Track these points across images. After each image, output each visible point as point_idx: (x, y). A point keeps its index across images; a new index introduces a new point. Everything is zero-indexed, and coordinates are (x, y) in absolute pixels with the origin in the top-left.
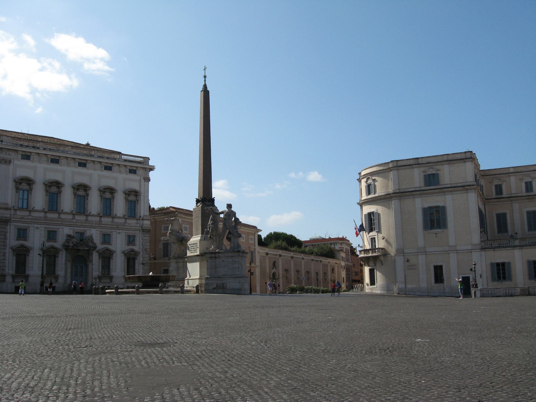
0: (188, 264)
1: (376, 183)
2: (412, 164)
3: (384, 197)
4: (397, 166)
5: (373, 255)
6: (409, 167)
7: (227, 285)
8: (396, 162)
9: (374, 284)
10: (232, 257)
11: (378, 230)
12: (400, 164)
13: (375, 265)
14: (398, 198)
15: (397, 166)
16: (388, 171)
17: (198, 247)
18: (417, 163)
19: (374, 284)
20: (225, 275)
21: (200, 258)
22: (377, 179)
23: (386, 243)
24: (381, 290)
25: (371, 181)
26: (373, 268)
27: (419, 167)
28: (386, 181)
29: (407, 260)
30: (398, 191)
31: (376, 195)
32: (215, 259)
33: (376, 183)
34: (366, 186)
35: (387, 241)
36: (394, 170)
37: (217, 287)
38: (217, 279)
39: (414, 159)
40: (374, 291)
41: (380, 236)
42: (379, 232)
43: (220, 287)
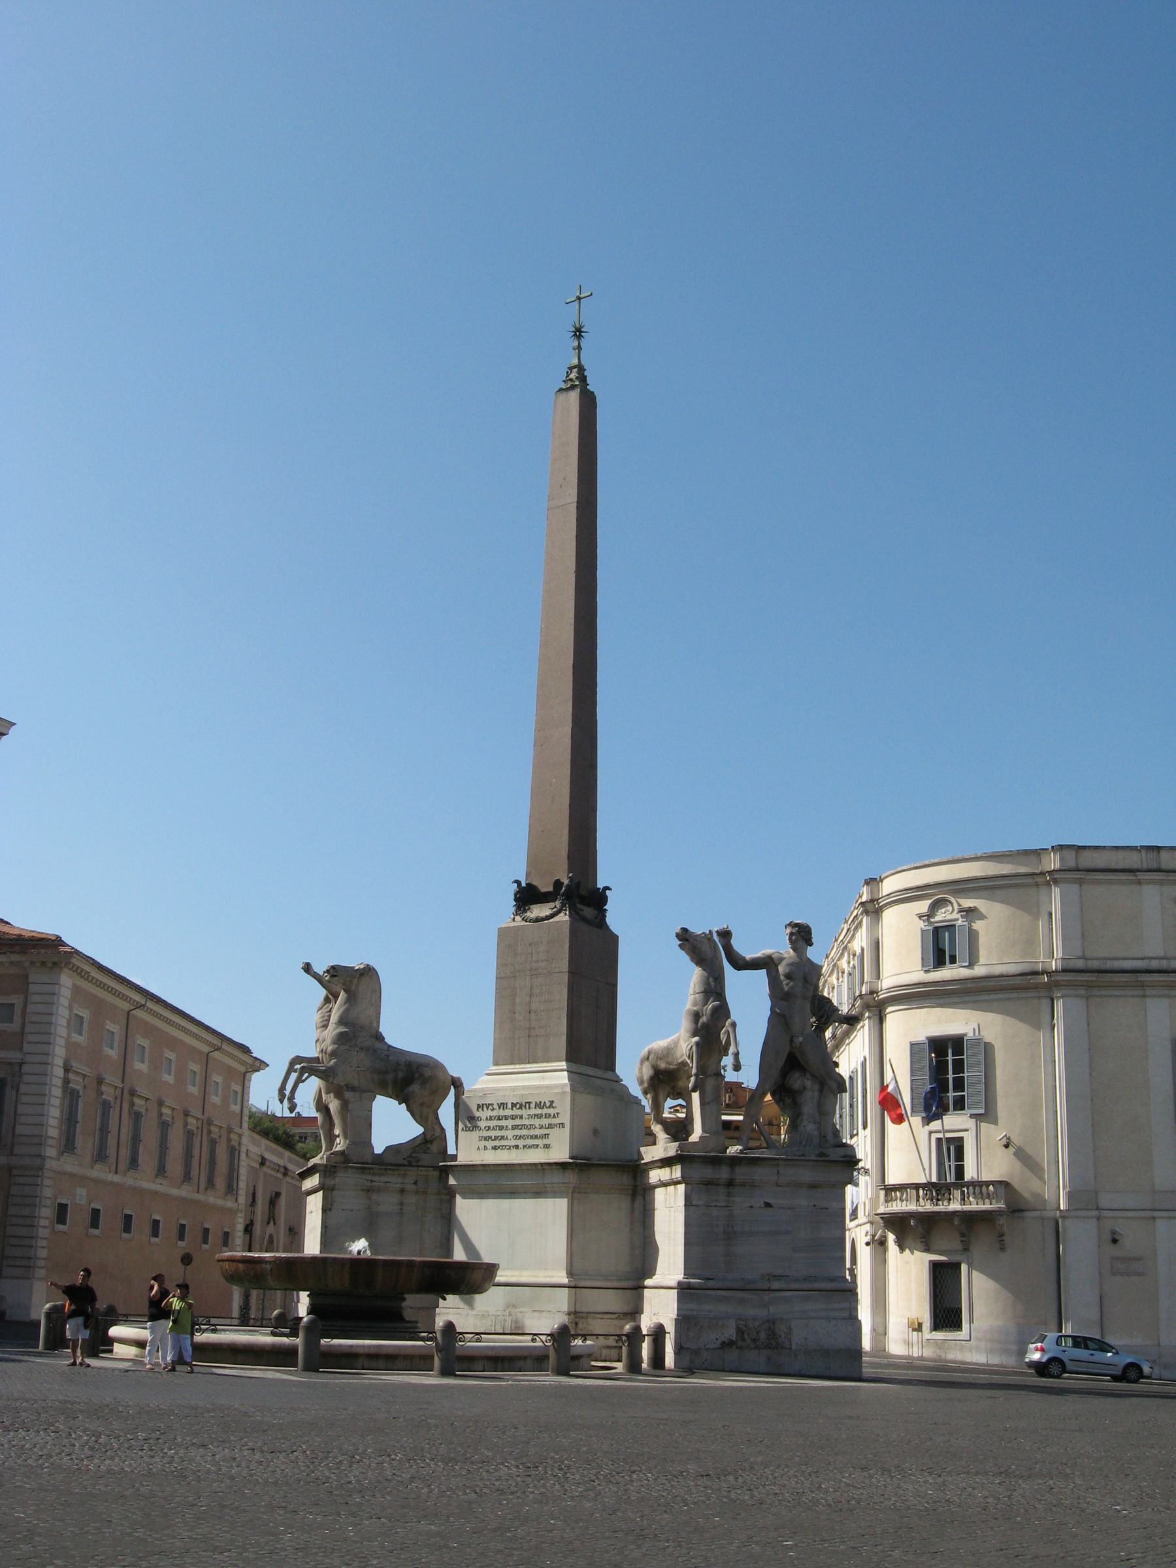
0: (459, 1199)
1: (978, 925)
2: (1135, 866)
3: (1018, 980)
4: (1077, 870)
5: (966, 1208)
6: (1123, 876)
7: (790, 1328)
8: (1073, 853)
9: (956, 1325)
10: (813, 1186)
11: (982, 1111)
12: (1087, 860)
13: (966, 1249)
14: (1082, 992)
15: (1077, 870)
16: (1037, 885)
17: (563, 1125)
18: (1154, 866)
19: (956, 1325)
20: (777, 1277)
21: (571, 1177)
22: (983, 910)
23: (1018, 1165)
24: (991, 1351)
25: (955, 915)
26: (955, 1258)
27: (1161, 883)
28: (1027, 918)
29: (1109, 1237)
30: (1080, 964)
31: (979, 971)
32: (729, 1195)
33: (978, 925)
34: (923, 931)
35: (1022, 1155)
36: (1066, 881)
37: (743, 1339)
38: (740, 1294)
39: (1143, 852)
40: (954, 1355)
41: (994, 1133)
42: (987, 1115)
43: (754, 1340)
